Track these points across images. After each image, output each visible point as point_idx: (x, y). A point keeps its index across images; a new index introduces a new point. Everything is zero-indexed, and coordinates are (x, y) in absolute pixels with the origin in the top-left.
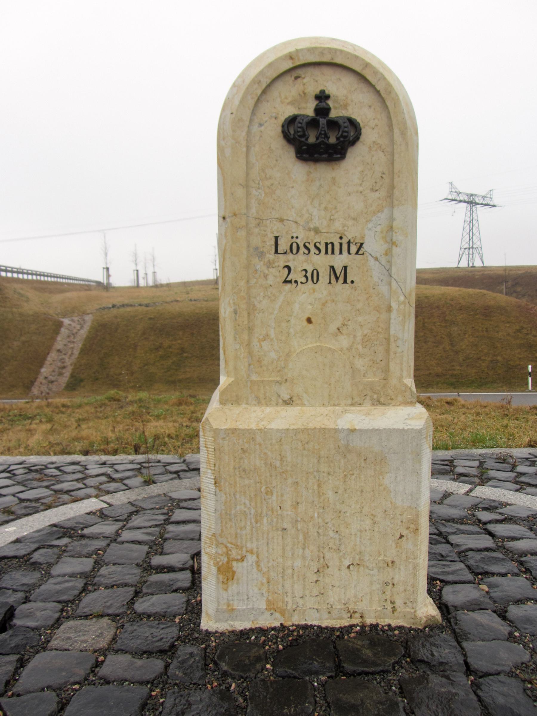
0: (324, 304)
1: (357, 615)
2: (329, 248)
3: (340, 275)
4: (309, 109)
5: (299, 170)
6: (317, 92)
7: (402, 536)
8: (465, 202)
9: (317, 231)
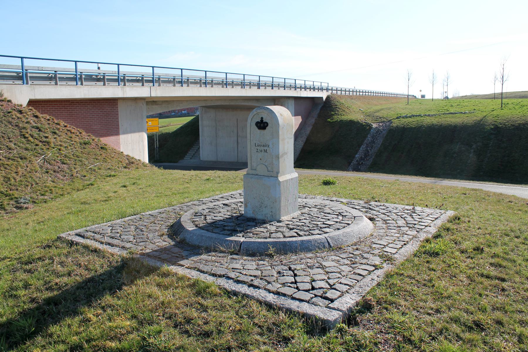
2: (264, 146)
3: (266, 151)
5: (259, 131)
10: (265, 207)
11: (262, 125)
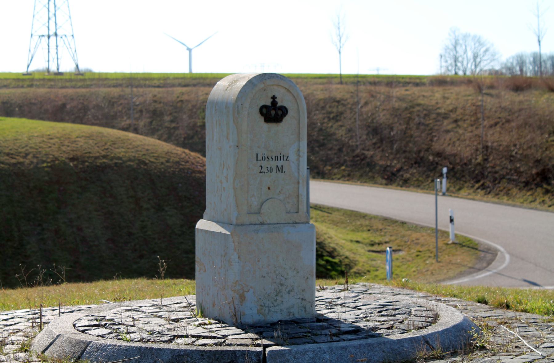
0: (274, 181)
1: (292, 314)
2: (276, 158)
3: (280, 169)
4: (268, 103)
5: (266, 126)
6: (272, 96)
7: (307, 278)
8: (480, 251)
9: (272, 151)
10: (289, 292)
11: (273, 112)
